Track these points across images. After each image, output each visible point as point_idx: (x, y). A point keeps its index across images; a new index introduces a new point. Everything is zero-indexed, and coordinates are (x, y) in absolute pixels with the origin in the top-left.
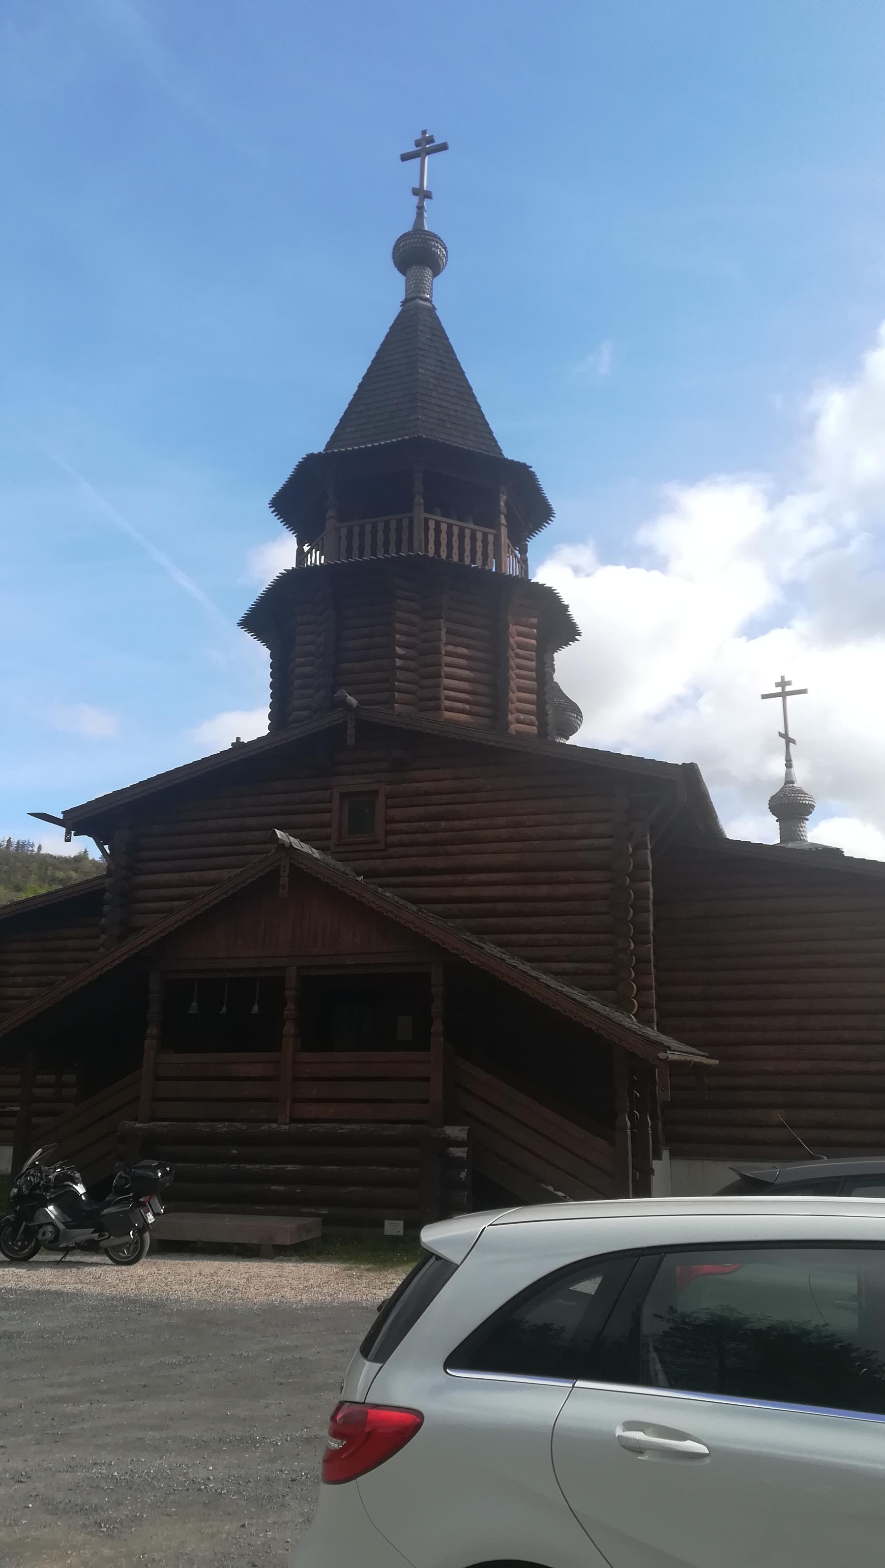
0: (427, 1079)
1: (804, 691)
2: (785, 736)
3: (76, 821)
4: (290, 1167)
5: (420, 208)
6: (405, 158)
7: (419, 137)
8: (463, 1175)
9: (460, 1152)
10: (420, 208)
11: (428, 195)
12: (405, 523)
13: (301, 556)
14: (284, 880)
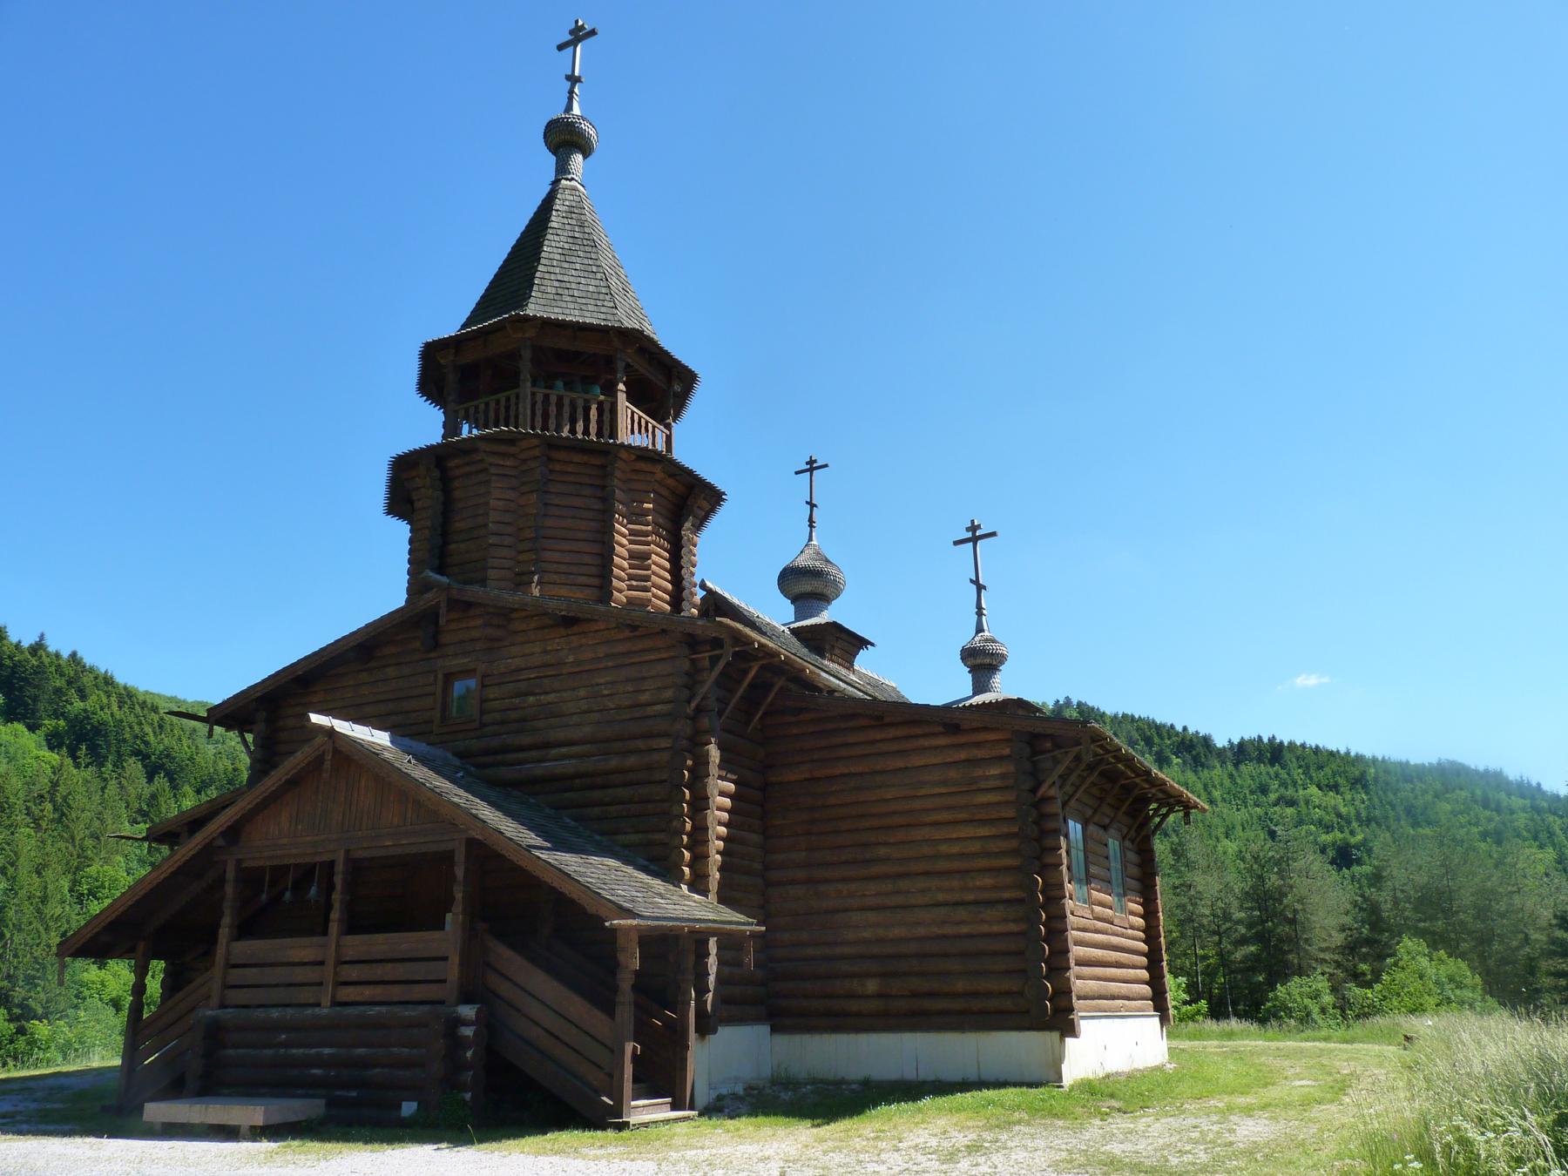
0: (445, 959)
1: (993, 534)
2: (976, 582)
4: (327, 1051)
6: (561, 47)
7: (573, 26)
9: (468, 1032)
13: (451, 428)
14: (327, 765)
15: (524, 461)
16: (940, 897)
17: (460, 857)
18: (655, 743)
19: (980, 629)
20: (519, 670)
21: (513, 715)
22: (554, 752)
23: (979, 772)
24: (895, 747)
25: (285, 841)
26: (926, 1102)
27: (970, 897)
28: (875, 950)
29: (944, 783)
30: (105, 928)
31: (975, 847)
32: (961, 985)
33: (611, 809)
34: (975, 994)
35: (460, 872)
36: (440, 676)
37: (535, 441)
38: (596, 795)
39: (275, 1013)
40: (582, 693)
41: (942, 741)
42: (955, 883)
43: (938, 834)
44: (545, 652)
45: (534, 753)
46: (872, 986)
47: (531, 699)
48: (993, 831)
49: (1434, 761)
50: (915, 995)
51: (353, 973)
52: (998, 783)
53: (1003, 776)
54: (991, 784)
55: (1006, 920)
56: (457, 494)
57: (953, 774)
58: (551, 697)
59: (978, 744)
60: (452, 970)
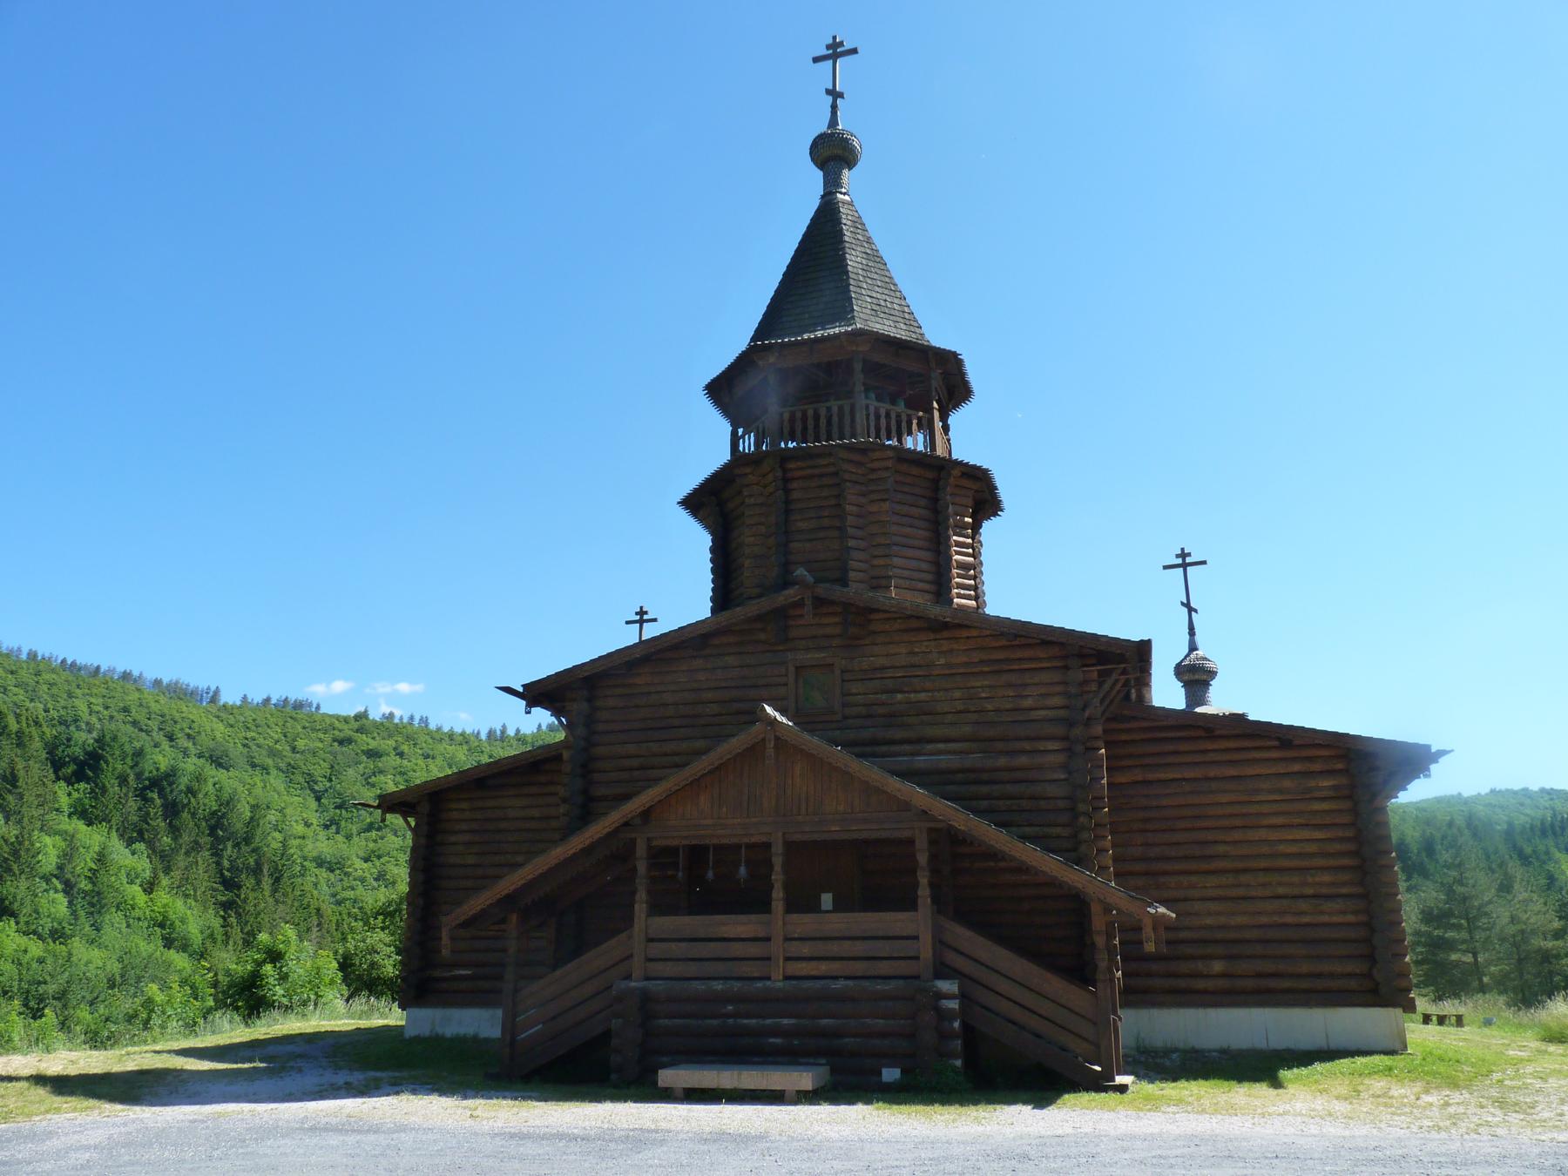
0: (916, 938)
2: (1187, 605)
3: (535, 694)
4: (785, 1021)
5: (834, 108)
6: (816, 60)
8: (956, 1024)
9: (953, 1005)
10: (834, 108)
11: (841, 95)
12: (847, 409)
14: (770, 751)
15: (873, 470)
16: (1281, 891)
17: (922, 843)
18: (1041, 746)
19: (1193, 648)
20: (884, 668)
21: (881, 710)
22: (930, 747)
23: (1312, 783)
24: (1228, 757)
25: (709, 822)
26: (1318, 1067)
27: (1310, 891)
28: (1220, 935)
29: (1281, 791)
30: (499, 901)
31: (1313, 848)
32: (1305, 968)
33: (1001, 803)
34: (1319, 975)
35: (923, 859)
36: (792, 669)
37: (890, 453)
38: (984, 789)
39: (718, 986)
40: (957, 694)
41: (1275, 754)
42: (1296, 879)
43: (1274, 835)
44: (912, 653)
45: (907, 748)
46: (1218, 967)
47: (899, 696)
48: (1329, 835)
49: (1484, 790)
50: (1259, 975)
51: (805, 949)
52: (1331, 793)
53: (1334, 787)
54: (1325, 793)
55: (1344, 913)
56: (795, 495)
57: (1287, 783)
58: (923, 696)
59: (1310, 759)
60: (926, 949)
